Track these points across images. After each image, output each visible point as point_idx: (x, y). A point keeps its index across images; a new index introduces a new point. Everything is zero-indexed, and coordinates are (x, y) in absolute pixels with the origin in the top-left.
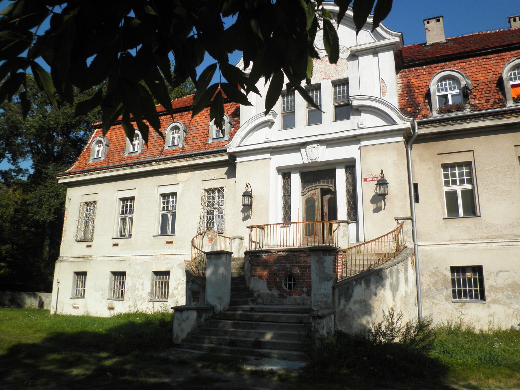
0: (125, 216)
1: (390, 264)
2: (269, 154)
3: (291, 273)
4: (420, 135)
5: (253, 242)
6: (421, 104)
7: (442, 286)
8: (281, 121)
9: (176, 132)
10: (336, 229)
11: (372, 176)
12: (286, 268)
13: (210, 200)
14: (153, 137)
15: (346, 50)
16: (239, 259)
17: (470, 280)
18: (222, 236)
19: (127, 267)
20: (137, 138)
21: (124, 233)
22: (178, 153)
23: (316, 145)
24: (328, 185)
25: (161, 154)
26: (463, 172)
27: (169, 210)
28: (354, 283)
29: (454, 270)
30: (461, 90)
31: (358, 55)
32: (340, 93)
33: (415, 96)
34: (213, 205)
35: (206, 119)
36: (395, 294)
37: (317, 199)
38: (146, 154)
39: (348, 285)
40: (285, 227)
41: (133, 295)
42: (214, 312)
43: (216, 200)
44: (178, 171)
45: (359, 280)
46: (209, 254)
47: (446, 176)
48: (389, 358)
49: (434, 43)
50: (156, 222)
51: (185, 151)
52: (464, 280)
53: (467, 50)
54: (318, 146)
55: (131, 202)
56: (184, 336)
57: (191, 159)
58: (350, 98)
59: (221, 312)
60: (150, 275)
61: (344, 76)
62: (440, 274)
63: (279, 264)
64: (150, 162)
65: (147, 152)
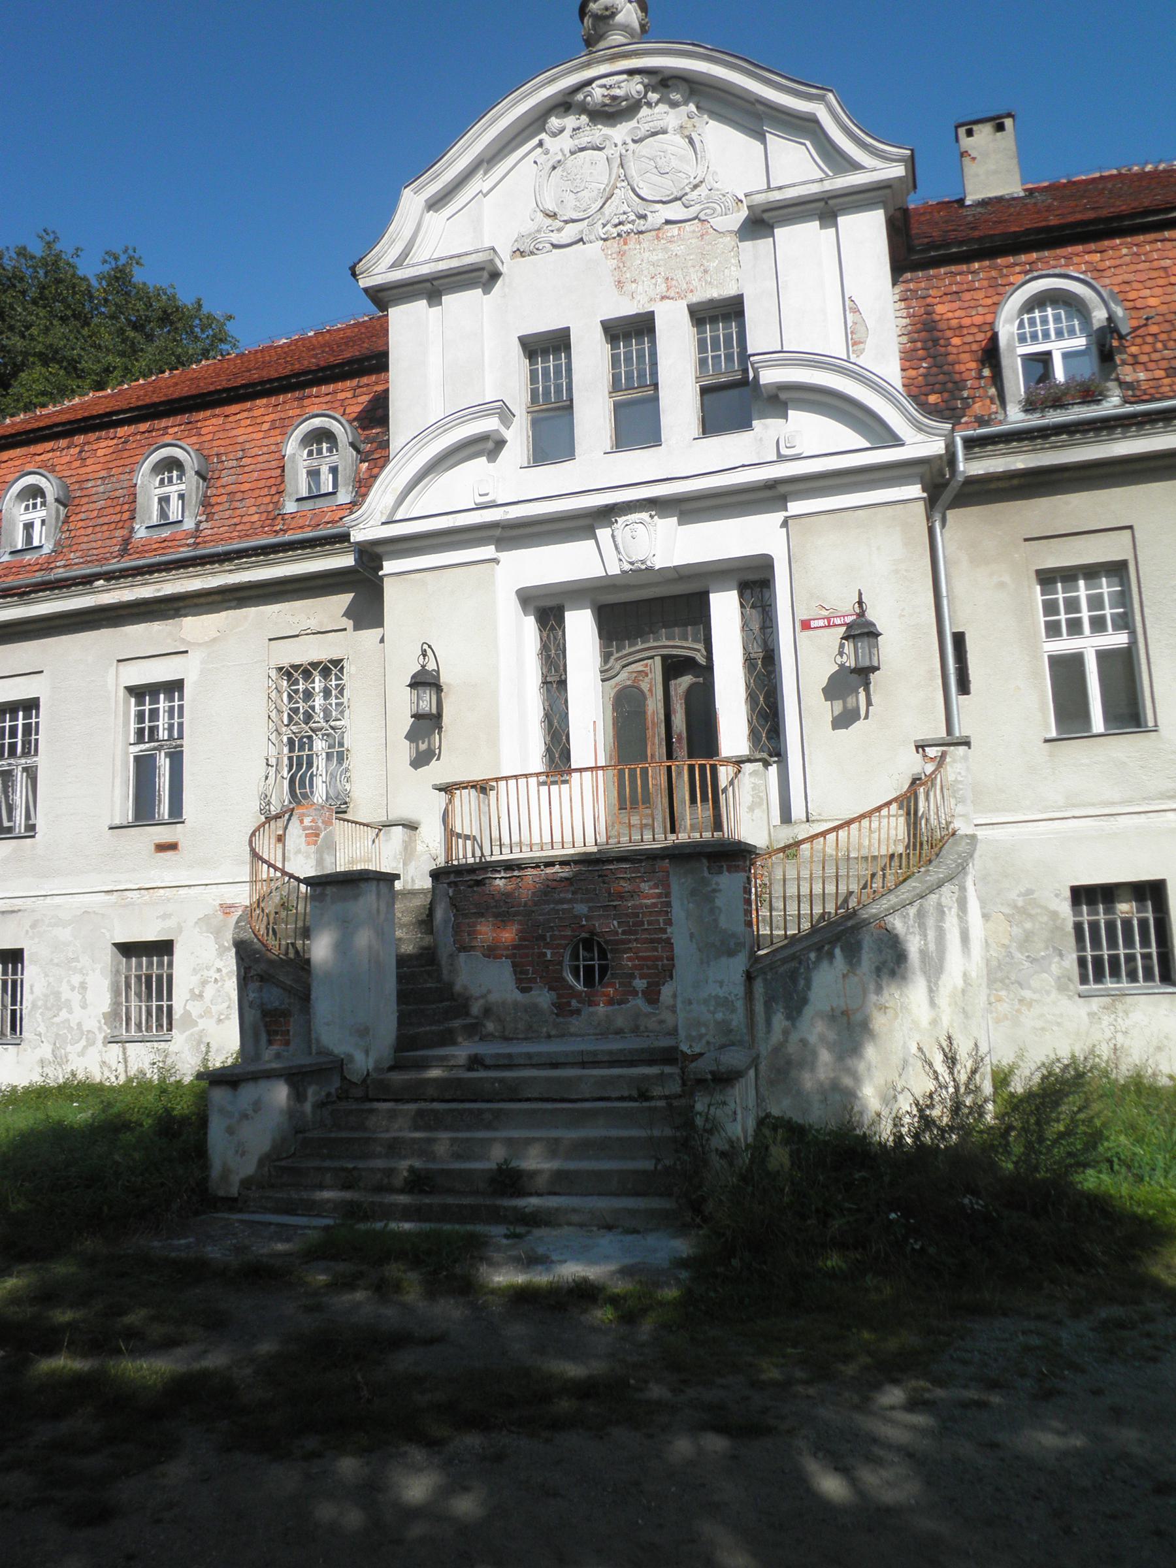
0: (10, 764)
1: (918, 891)
2: (492, 547)
3: (592, 933)
4: (971, 481)
5: (459, 836)
6: (969, 383)
7: (1047, 948)
8: (528, 437)
9: (170, 480)
10: (731, 783)
11: (825, 613)
12: (576, 917)
13: (297, 702)
14: (94, 498)
15: (734, 204)
16: (413, 893)
17: (1127, 923)
18: (344, 820)
19: (27, 931)
20: (39, 500)
21: (10, 819)
22: (182, 549)
23: (644, 516)
24: (685, 646)
25: (124, 551)
26: (1101, 595)
27: (158, 741)
28: (813, 956)
29: (1082, 895)
30: (1094, 337)
31: (771, 221)
32: (716, 347)
33: (951, 358)
34: (308, 717)
35: (272, 433)
36: (936, 984)
37: (650, 690)
38: (72, 556)
39: (794, 964)
40: (555, 783)
41: (53, 1023)
42: (344, 1078)
43: (318, 701)
44: (185, 607)
45: (826, 948)
46: (323, 885)
47: (1050, 608)
48: (972, 1208)
49: (990, 198)
50: (118, 781)
51: (205, 542)
52: (1110, 926)
53: (1104, 213)
54: (652, 517)
55: (27, 716)
56: (247, 1167)
57: (227, 566)
58: (752, 359)
59: (368, 1074)
60: (107, 955)
61: (730, 291)
62: (1039, 911)
63: (552, 906)
64: (86, 581)
65: (74, 548)
